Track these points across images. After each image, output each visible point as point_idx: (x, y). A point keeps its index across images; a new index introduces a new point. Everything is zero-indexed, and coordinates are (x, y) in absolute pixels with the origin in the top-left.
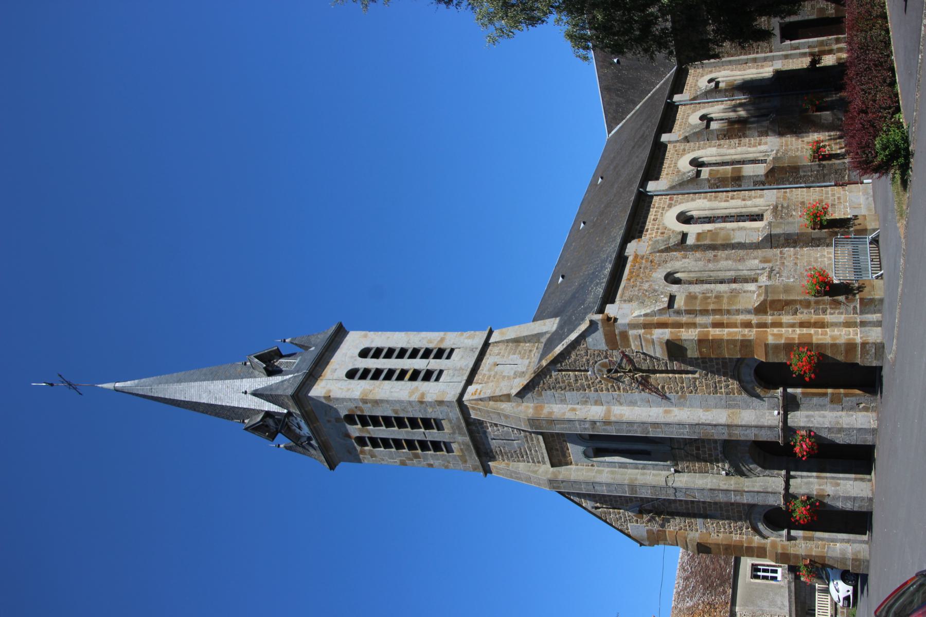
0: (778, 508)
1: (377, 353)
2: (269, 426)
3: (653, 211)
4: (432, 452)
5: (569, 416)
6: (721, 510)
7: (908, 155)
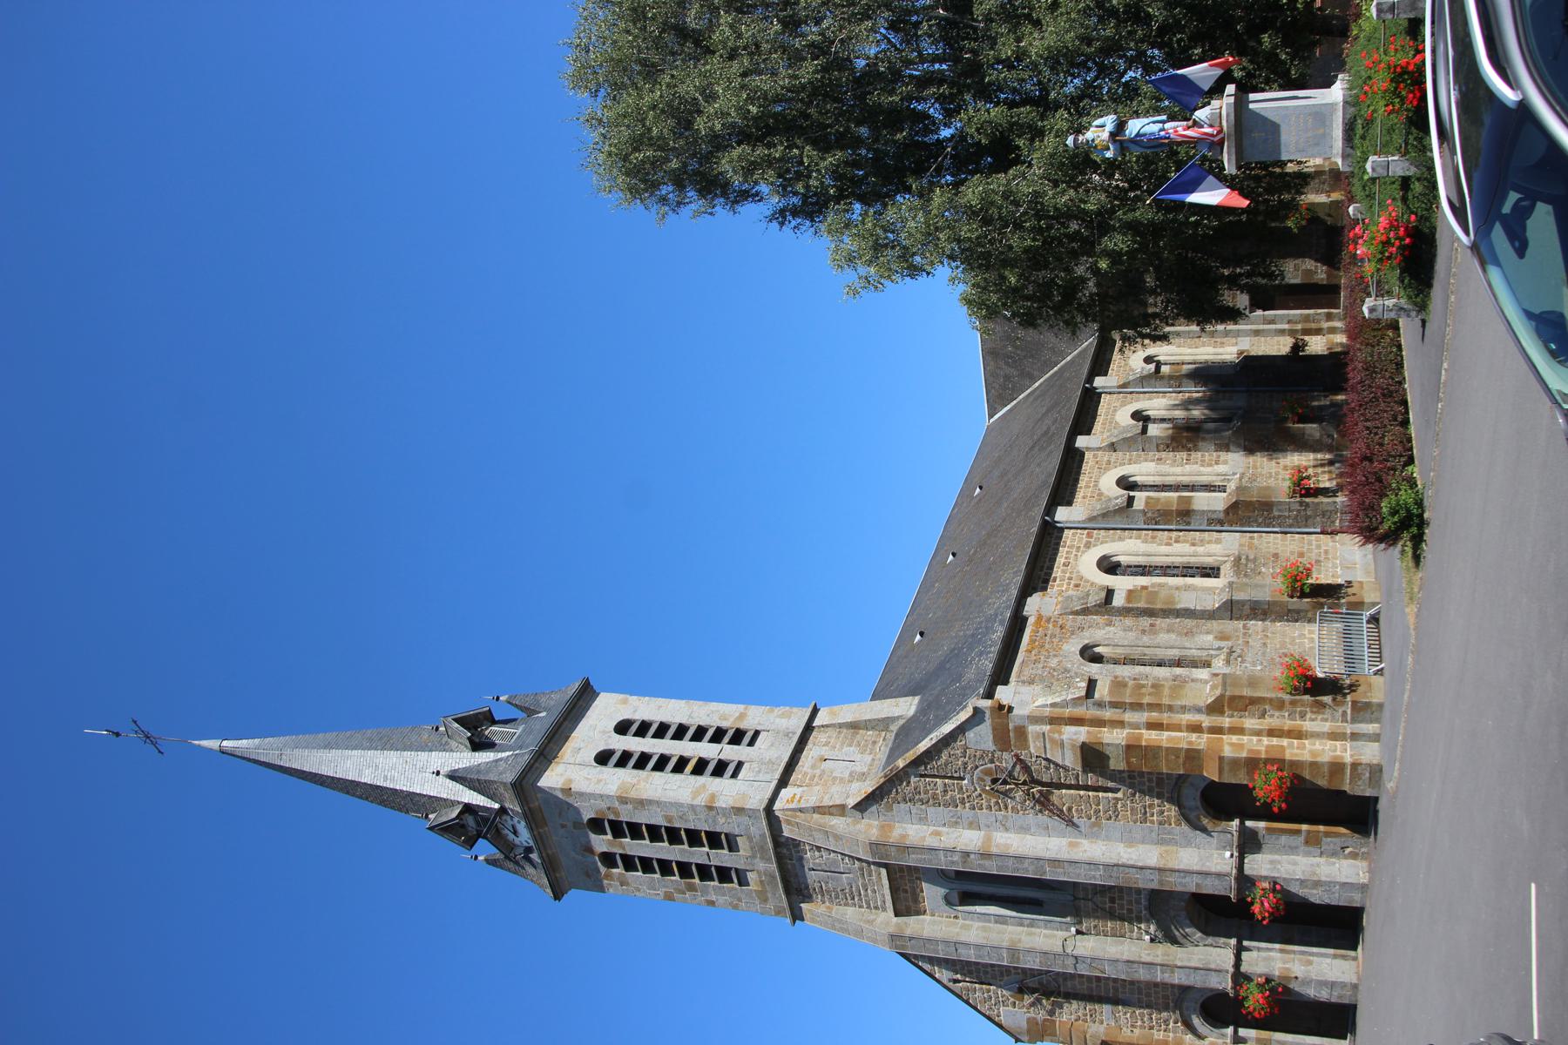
0: (1223, 995)
1: (643, 729)
2: (468, 827)
3: (1063, 551)
4: (716, 883)
5: (931, 842)
6: (1140, 992)
7: (1422, 524)
